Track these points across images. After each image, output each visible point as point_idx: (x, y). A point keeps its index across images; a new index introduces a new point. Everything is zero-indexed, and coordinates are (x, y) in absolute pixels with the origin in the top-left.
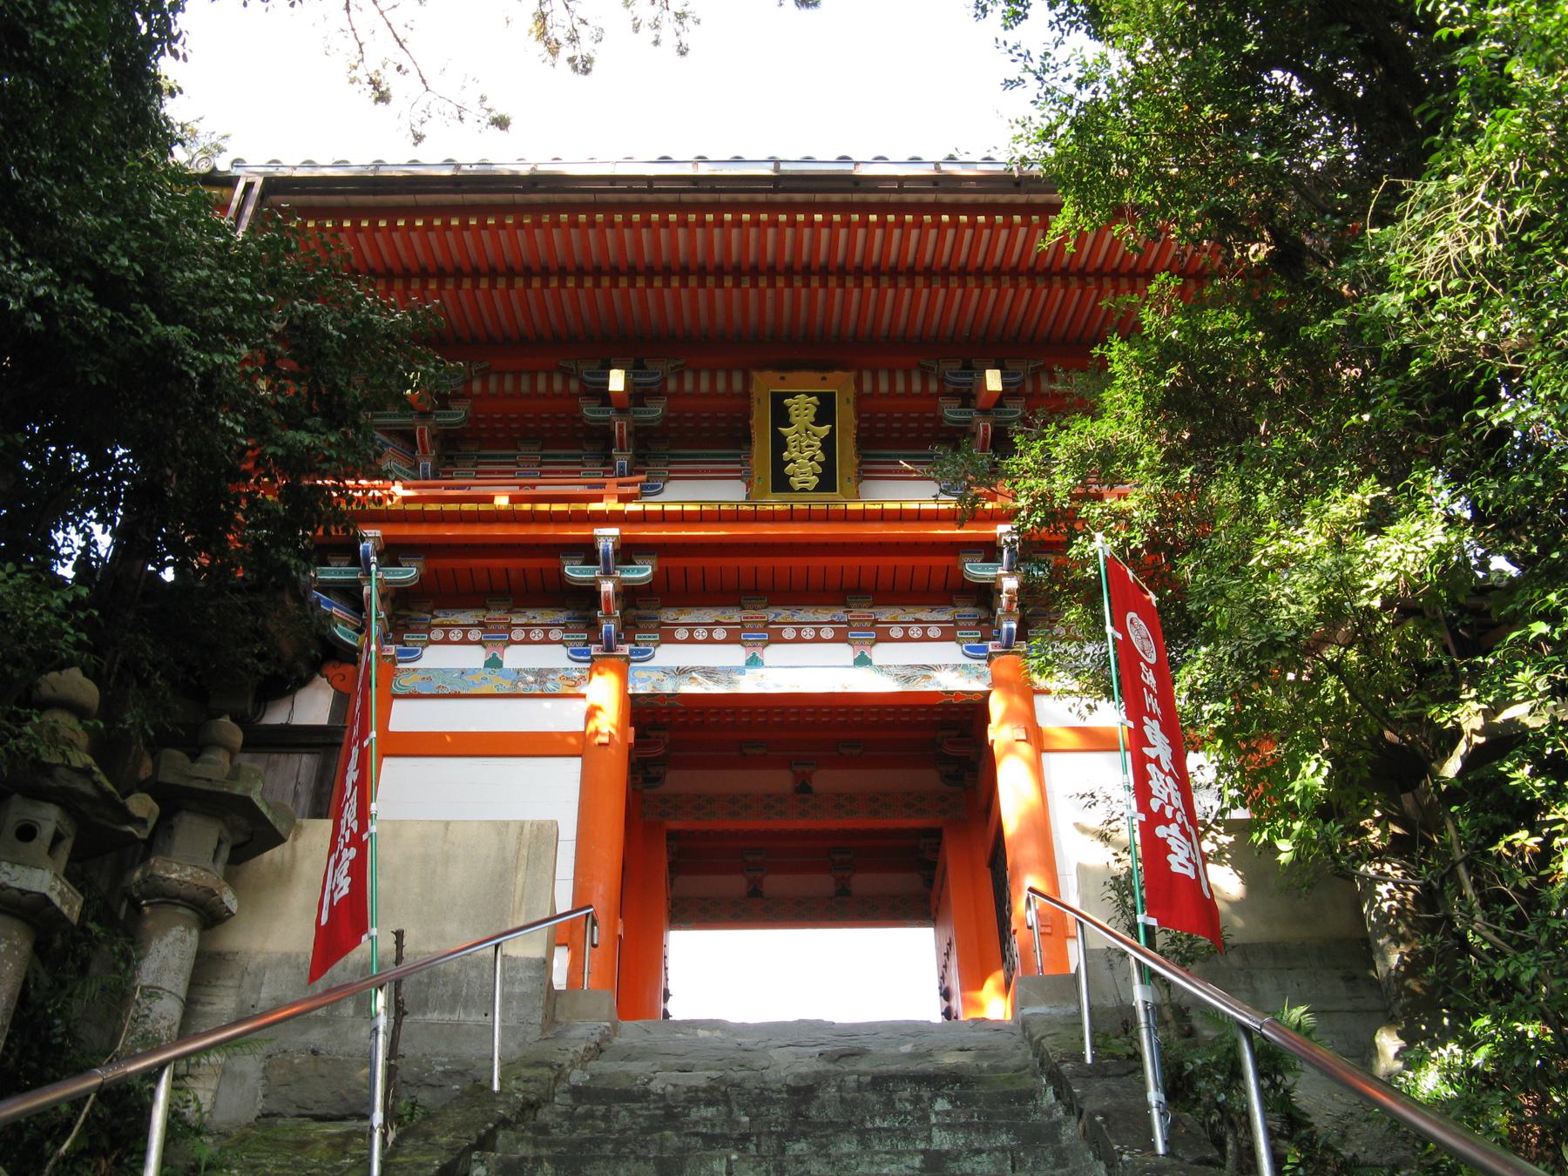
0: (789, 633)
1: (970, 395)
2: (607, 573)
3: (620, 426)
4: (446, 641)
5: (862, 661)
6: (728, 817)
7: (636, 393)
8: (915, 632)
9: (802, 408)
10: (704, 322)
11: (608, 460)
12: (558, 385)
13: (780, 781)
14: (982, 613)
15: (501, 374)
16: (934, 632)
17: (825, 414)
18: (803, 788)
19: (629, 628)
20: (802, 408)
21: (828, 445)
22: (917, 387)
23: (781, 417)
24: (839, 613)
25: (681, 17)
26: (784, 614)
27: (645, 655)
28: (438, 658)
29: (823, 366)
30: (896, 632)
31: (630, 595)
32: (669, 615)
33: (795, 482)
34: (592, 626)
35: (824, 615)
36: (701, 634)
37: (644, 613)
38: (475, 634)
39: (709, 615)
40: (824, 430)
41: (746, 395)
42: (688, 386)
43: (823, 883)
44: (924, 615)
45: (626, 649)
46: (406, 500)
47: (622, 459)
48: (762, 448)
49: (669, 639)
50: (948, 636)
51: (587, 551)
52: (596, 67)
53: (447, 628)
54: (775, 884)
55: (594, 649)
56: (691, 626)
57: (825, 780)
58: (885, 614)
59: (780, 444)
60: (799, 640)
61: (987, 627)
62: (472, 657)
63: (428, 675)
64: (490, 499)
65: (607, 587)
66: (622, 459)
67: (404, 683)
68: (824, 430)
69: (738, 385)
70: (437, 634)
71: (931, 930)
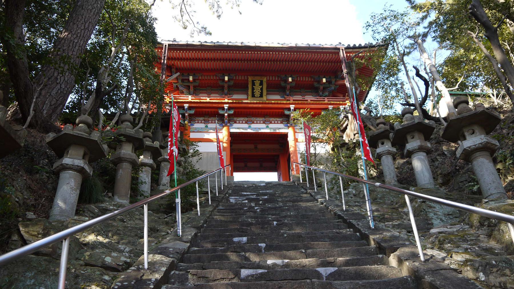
0: (238, 122)
1: (320, 82)
2: (226, 112)
3: (226, 85)
4: (198, 123)
5: (267, 127)
6: (248, 152)
7: (194, 80)
8: (276, 122)
9: (257, 83)
10: (209, 67)
11: (223, 90)
12: (215, 78)
13: (252, 146)
14: (287, 119)
15: (205, 76)
16: (279, 122)
17: (261, 84)
18: (256, 147)
19: (229, 121)
20: (257, 83)
21: (262, 89)
22: (277, 79)
23: (253, 84)
24: (264, 119)
25: (385, 11)
26: (273, 119)
27: (193, 125)
28: (197, 126)
29: (261, 76)
30: (273, 122)
31: (190, 115)
32: (235, 119)
33: (256, 96)
34: (223, 121)
35: (261, 119)
36: (241, 122)
37: (232, 119)
38: (203, 122)
39: (242, 119)
40: (261, 87)
41: (247, 80)
42: (237, 78)
43: (257, 164)
44: (278, 119)
45: (229, 124)
46: (192, 99)
47: (226, 91)
48: (250, 92)
49: (235, 123)
50: (281, 123)
51: (223, 109)
52: (217, 19)
53: (198, 120)
54: (250, 164)
55: (223, 124)
56: (239, 121)
57: (260, 146)
58: (271, 119)
59: (253, 89)
60: (257, 123)
61: (223, 121)
62: (203, 125)
63: (196, 128)
64: (206, 99)
65: (226, 114)
66: (226, 91)
67: (192, 130)
68: (261, 87)
69: (246, 78)
70: (197, 122)
71: (276, 173)
